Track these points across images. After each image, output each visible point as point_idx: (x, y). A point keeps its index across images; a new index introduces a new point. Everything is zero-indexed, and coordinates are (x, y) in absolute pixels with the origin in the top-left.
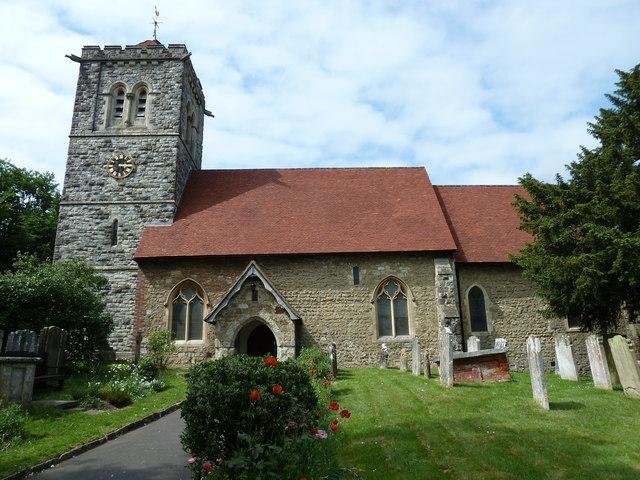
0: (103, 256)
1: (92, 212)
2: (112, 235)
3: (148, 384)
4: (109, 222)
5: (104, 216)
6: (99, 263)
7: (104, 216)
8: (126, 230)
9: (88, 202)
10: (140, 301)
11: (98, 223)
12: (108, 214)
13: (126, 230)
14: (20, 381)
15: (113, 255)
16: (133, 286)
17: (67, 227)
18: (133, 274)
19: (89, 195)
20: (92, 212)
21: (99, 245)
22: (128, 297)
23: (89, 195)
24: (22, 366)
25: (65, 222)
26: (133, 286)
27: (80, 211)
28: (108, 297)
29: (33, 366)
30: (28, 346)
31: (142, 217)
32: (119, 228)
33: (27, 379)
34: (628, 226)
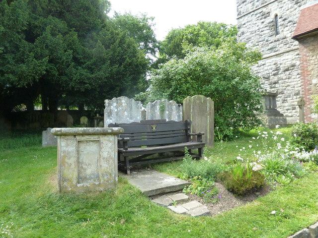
0: (271, 46)
1: (257, 16)
2: (274, 26)
3: (306, 155)
4: (271, 18)
5: (266, 15)
6: (268, 52)
7: (266, 15)
8: (285, 19)
9: (255, 9)
10: (304, 73)
11: (263, 22)
12: (269, 13)
13: (285, 19)
14: (97, 156)
15: (278, 43)
16: (298, 63)
17: (243, 33)
18: (296, 53)
19: (253, 5)
20: (257, 16)
21: (266, 39)
22: (295, 73)
23: (253, 5)
24: (95, 138)
25: (242, 30)
26: (298, 63)
27: (250, 19)
28: (279, 76)
29: (112, 138)
30: (170, 115)
31: (297, 3)
32: (279, 20)
33: (105, 154)
34: (310, 148)
